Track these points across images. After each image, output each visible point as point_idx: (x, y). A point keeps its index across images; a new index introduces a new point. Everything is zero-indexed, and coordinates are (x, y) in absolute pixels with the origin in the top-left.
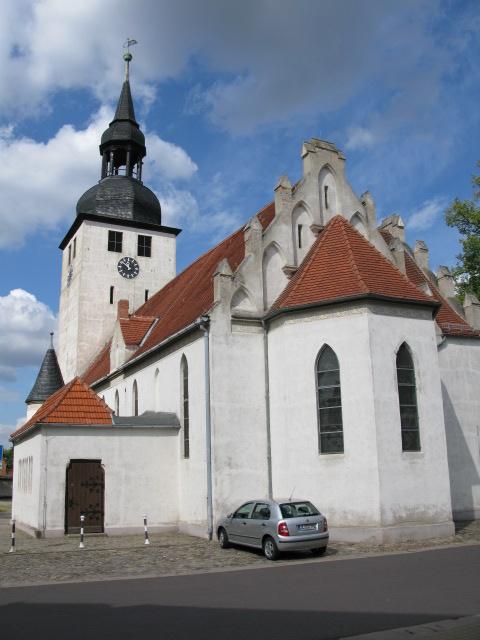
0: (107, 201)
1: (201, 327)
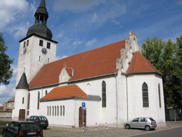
0: (39, 31)
1: (116, 75)
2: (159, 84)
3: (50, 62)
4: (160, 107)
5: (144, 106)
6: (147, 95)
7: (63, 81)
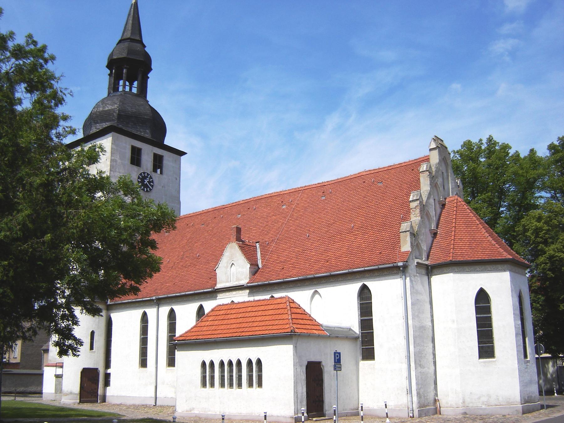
5: (481, 356)
6: (490, 325)
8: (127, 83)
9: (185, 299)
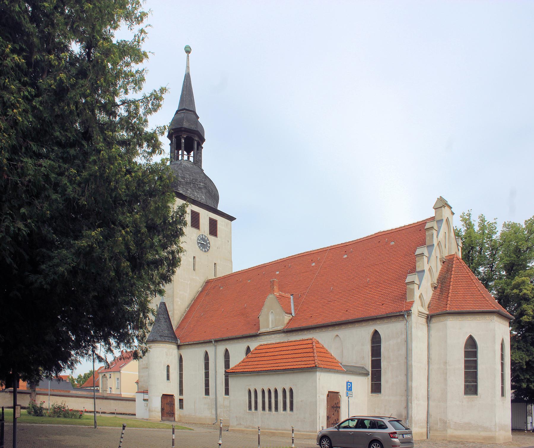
2: (503, 340)
3: (220, 274)
4: (503, 394)
5: (466, 393)
6: (476, 367)
7: (270, 326)
8: (185, 153)
9: (343, 327)
